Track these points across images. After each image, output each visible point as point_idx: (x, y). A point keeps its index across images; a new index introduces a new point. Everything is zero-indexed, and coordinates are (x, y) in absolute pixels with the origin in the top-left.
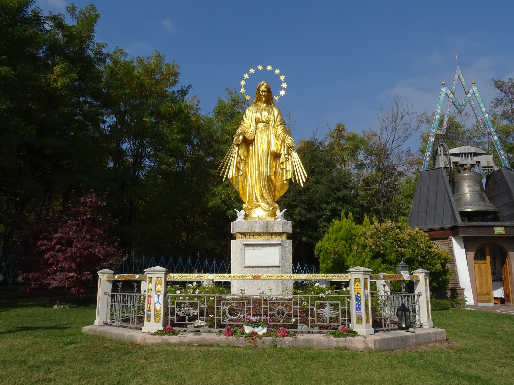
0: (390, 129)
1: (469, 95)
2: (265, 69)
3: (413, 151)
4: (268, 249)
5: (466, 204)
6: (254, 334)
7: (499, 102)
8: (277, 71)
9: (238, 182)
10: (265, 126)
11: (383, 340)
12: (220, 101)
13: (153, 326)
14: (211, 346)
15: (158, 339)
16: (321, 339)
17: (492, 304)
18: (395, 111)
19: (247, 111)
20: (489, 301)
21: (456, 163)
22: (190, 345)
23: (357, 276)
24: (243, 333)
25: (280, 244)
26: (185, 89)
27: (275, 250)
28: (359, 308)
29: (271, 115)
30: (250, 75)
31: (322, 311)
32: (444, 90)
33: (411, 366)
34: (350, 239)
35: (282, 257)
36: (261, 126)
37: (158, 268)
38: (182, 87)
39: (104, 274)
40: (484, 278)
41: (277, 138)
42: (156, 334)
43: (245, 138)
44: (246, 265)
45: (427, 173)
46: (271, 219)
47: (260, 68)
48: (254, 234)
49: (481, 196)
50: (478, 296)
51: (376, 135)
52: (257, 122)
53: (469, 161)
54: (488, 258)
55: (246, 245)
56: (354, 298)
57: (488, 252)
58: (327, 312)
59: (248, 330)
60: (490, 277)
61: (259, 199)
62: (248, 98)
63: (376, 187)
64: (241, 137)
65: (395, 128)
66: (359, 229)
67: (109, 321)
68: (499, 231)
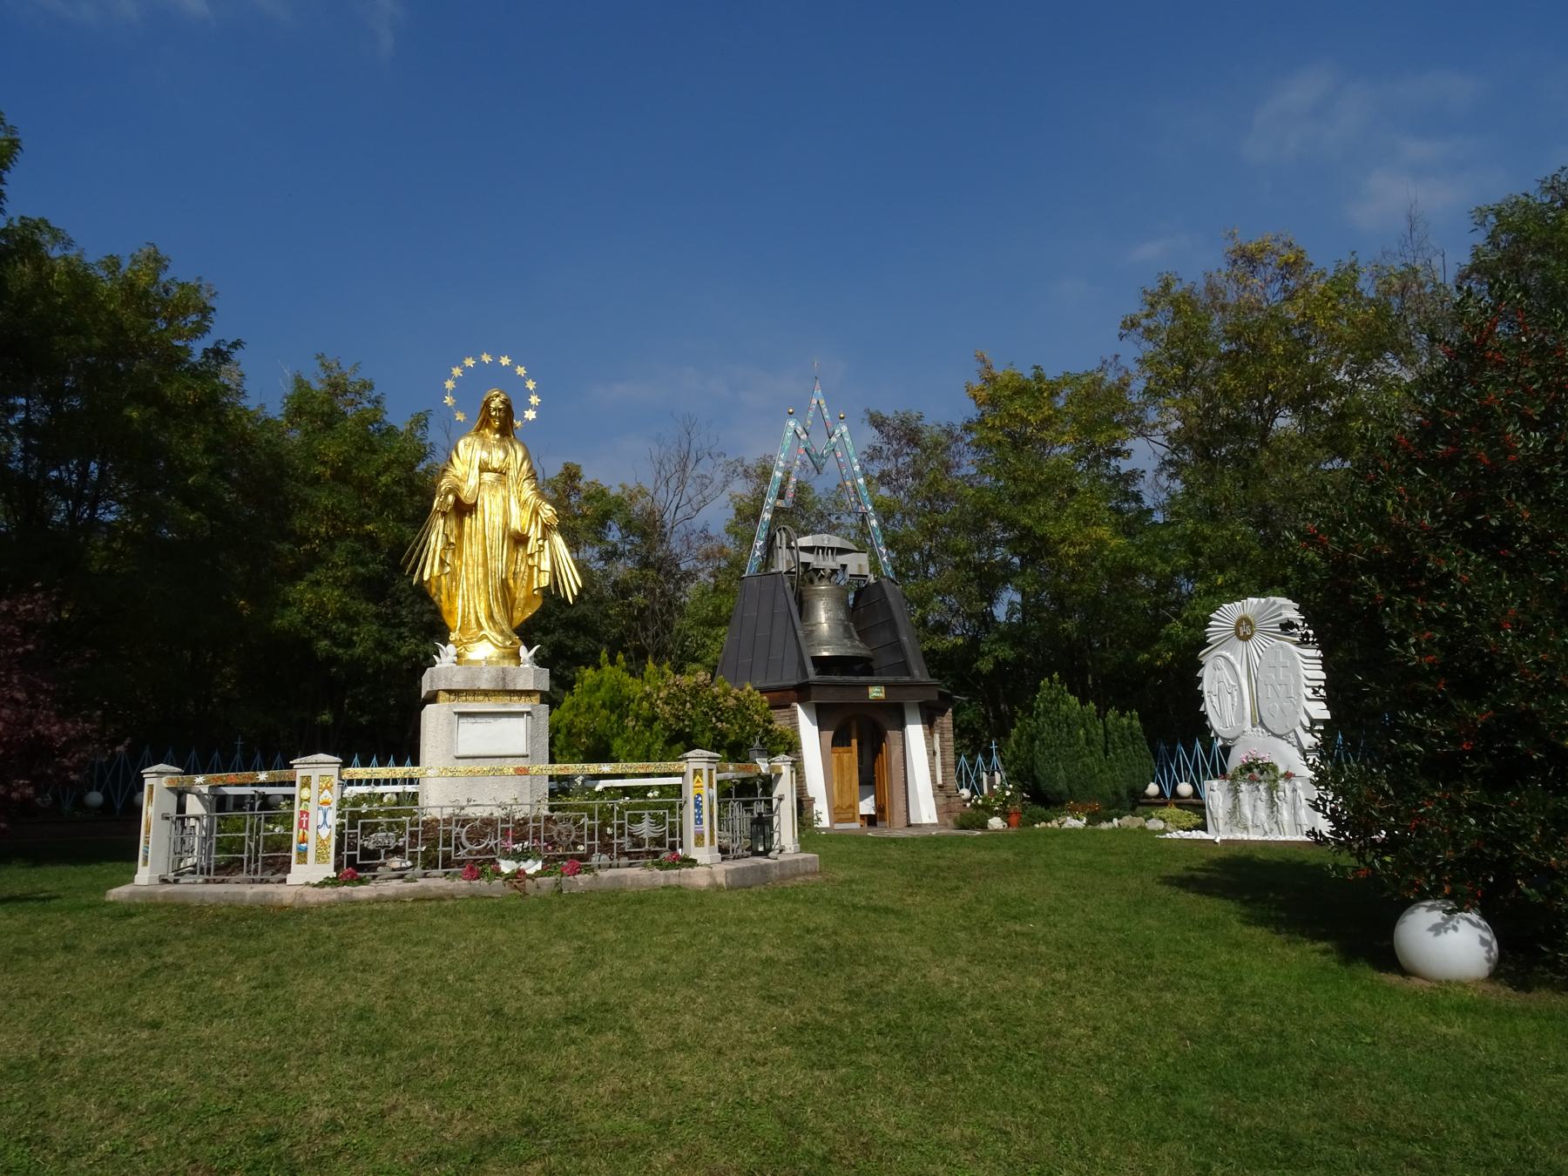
0: (673, 483)
1: (834, 439)
2: (496, 363)
3: (712, 532)
4: (504, 721)
5: (820, 644)
6: (519, 873)
7: (874, 454)
8: (521, 371)
9: (439, 589)
10: (498, 480)
11: (737, 870)
12: (299, 382)
13: (310, 872)
14: (440, 898)
15: (330, 894)
16: (638, 875)
17: (856, 825)
18: (685, 446)
19: (461, 444)
20: (853, 820)
21: (806, 565)
22: (397, 899)
23: (697, 766)
24: (498, 873)
25: (528, 713)
26: (224, 348)
27: (520, 724)
28: (699, 821)
29: (511, 459)
30: (466, 370)
31: (636, 828)
32: (792, 424)
33: (795, 901)
34: (618, 705)
35: (532, 739)
36: (488, 477)
37: (322, 757)
38: (218, 343)
39: (160, 774)
40: (847, 778)
41: (523, 504)
42: (322, 884)
43: (458, 500)
44: (461, 753)
45: (755, 581)
46: (509, 665)
47: (486, 358)
48: (474, 693)
49: (847, 629)
50: (837, 813)
51: (645, 494)
52: (484, 468)
53: (829, 563)
54: (854, 742)
55: (462, 715)
56: (692, 802)
57: (854, 732)
58: (646, 829)
59: (506, 867)
60: (856, 776)
61: (483, 621)
62: (460, 417)
63: (638, 599)
64: (451, 498)
65: (682, 482)
66: (634, 687)
67: (171, 876)
68: (876, 693)
